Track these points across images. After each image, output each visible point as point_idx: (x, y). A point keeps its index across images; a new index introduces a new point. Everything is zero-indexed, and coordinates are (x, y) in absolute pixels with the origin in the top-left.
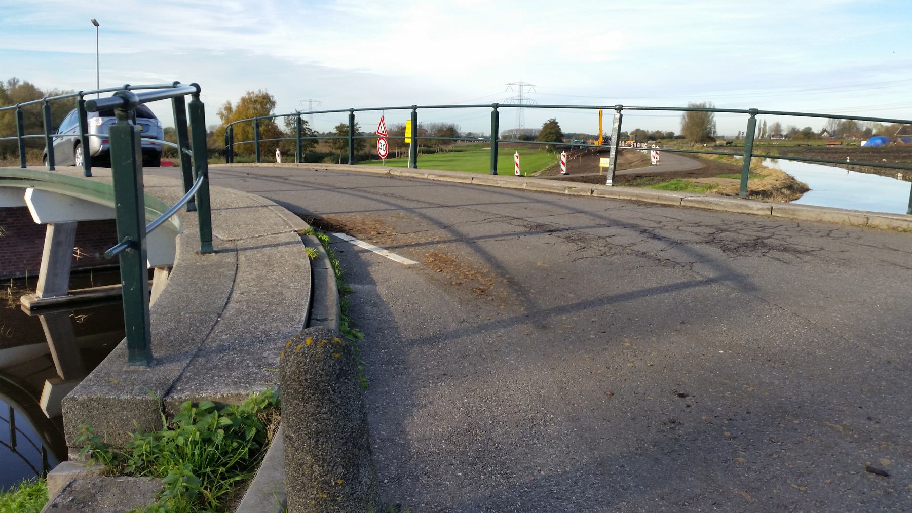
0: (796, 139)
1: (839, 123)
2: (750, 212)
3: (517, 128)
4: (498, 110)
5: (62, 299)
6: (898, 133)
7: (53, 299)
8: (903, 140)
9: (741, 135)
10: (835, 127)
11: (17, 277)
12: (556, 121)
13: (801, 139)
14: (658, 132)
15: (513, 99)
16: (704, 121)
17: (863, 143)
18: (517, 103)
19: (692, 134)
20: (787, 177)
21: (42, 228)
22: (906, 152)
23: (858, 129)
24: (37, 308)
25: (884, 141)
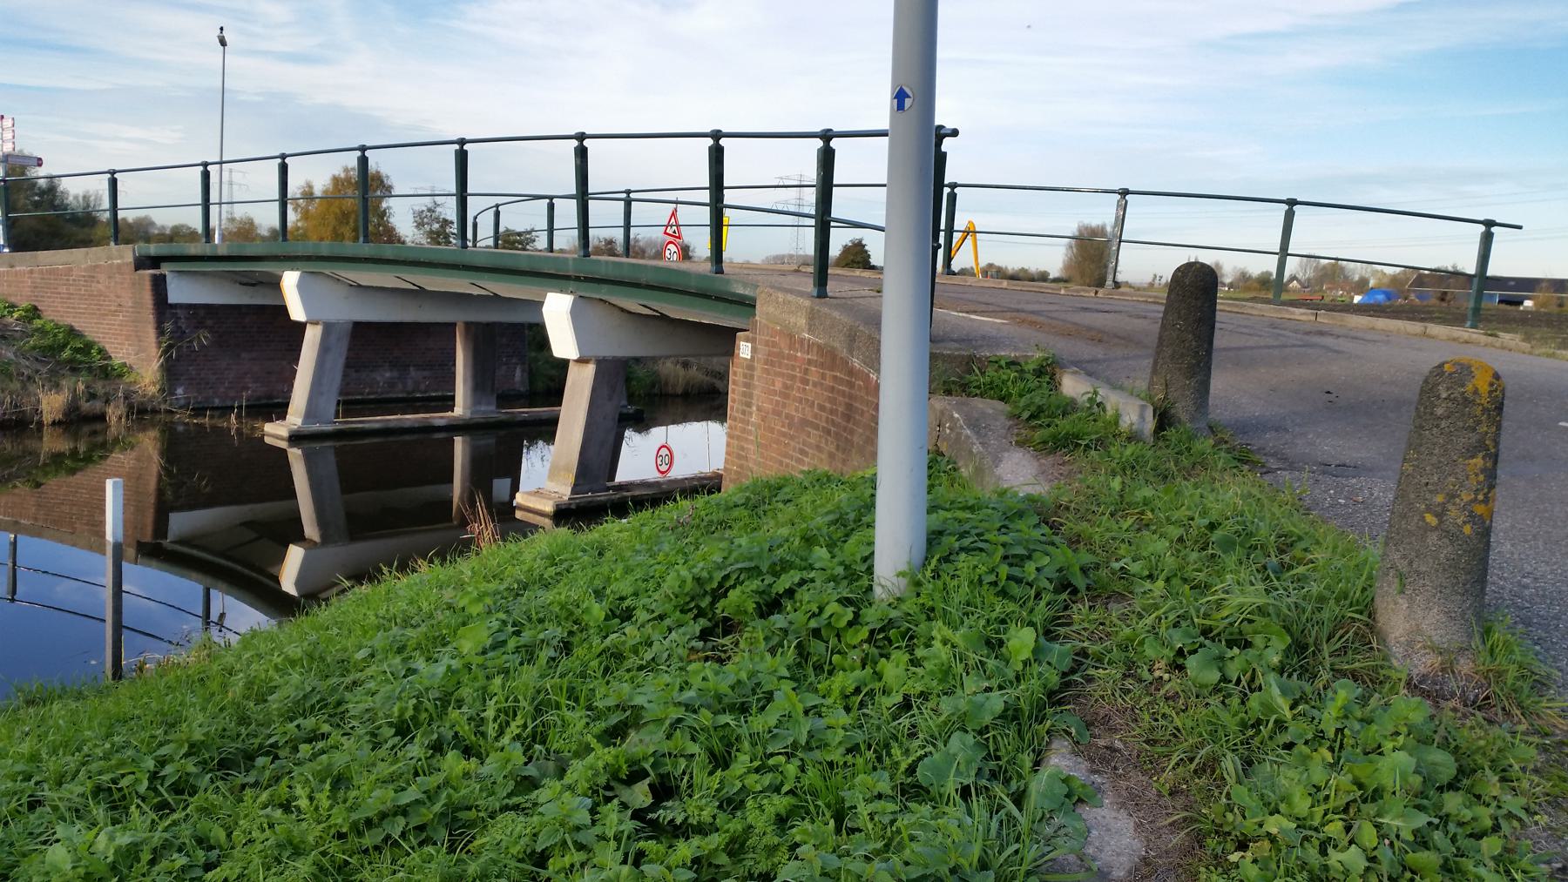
0: (1248, 289)
1: (1316, 267)
2: (1292, 317)
3: (792, 252)
4: (956, 190)
5: (329, 428)
6: (1411, 286)
7: (316, 427)
8: (1418, 297)
9: (1157, 281)
10: (1310, 273)
11: (216, 405)
12: (864, 242)
13: (1255, 289)
14: (1023, 270)
15: (786, 203)
16: (1102, 254)
17: (1357, 299)
18: (792, 209)
19: (1082, 275)
20: (860, 620)
21: (300, 328)
22: (1424, 313)
23: (1346, 278)
24: (296, 438)
25: (1389, 296)
